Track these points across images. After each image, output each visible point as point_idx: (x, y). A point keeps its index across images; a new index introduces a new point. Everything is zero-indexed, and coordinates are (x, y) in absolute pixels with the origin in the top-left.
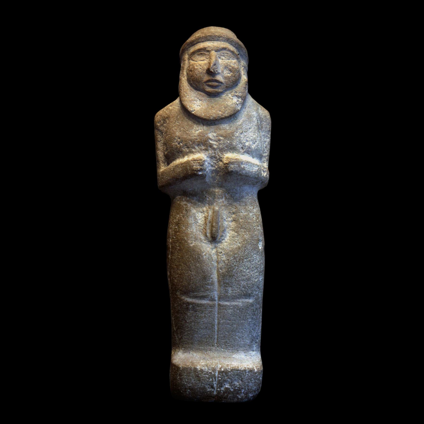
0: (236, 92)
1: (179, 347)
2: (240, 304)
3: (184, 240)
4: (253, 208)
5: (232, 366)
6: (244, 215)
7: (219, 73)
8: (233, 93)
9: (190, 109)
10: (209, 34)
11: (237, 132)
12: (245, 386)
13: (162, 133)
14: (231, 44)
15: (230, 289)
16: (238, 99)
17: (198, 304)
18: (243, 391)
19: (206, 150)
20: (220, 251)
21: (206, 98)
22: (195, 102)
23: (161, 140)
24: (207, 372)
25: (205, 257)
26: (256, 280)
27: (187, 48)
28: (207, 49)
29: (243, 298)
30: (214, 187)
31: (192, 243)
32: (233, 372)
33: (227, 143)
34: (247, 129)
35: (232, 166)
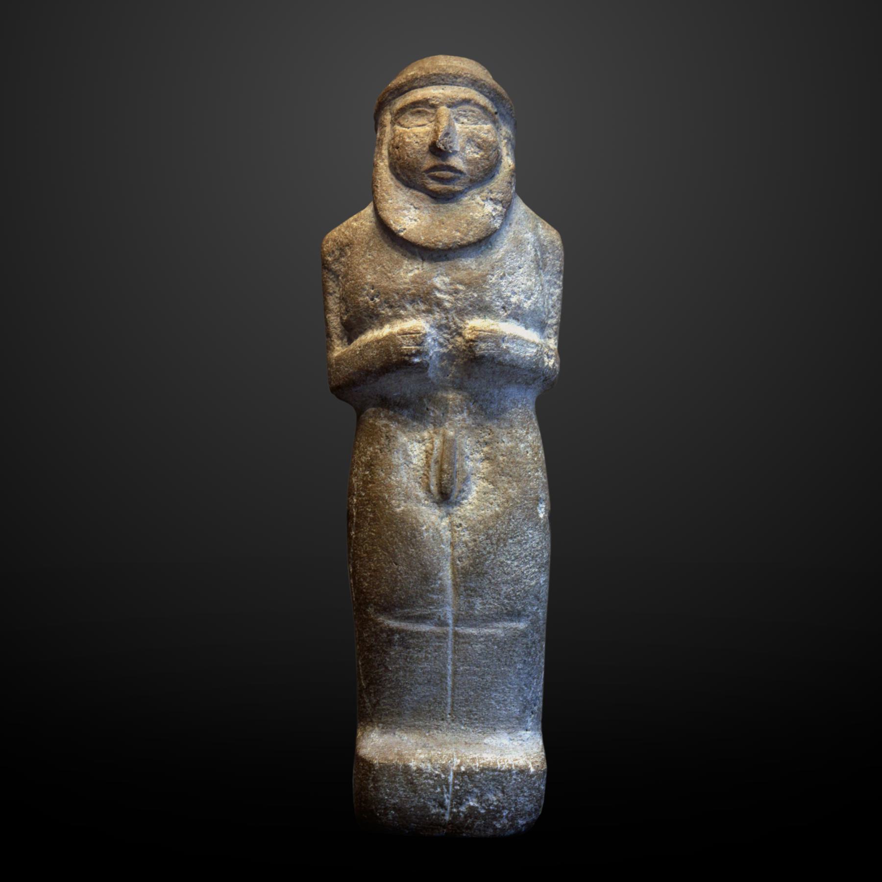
0: (491, 192)
1: (372, 721)
2: (500, 633)
3: (383, 499)
4: (527, 433)
5: (482, 762)
6: (507, 448)
7: (455, 152)
8: (484, 194)
9: (396, 227)
10: (434, 72)
11: (493, 275)
12: (510, 804)
13: (338, 276)
14: (481, 92)
15: (478, 601)
16: (495, 206)
17: (412, 632)
18: (505, 813)
19: (429, 312)
20: (458, 521)
21: (428, 203)
22: (405, 212)
23: (335, 292)
24: (431, 774)
25: (426, 535)
26: (533, 583)
27: (390, 100)
28: (431, 102)
29: (505, 620)
30: (445, 389)
31: (399, 507)
32: (485, 774)
33: (473, 297)
34: (514, 268)
35: (483, 345)
